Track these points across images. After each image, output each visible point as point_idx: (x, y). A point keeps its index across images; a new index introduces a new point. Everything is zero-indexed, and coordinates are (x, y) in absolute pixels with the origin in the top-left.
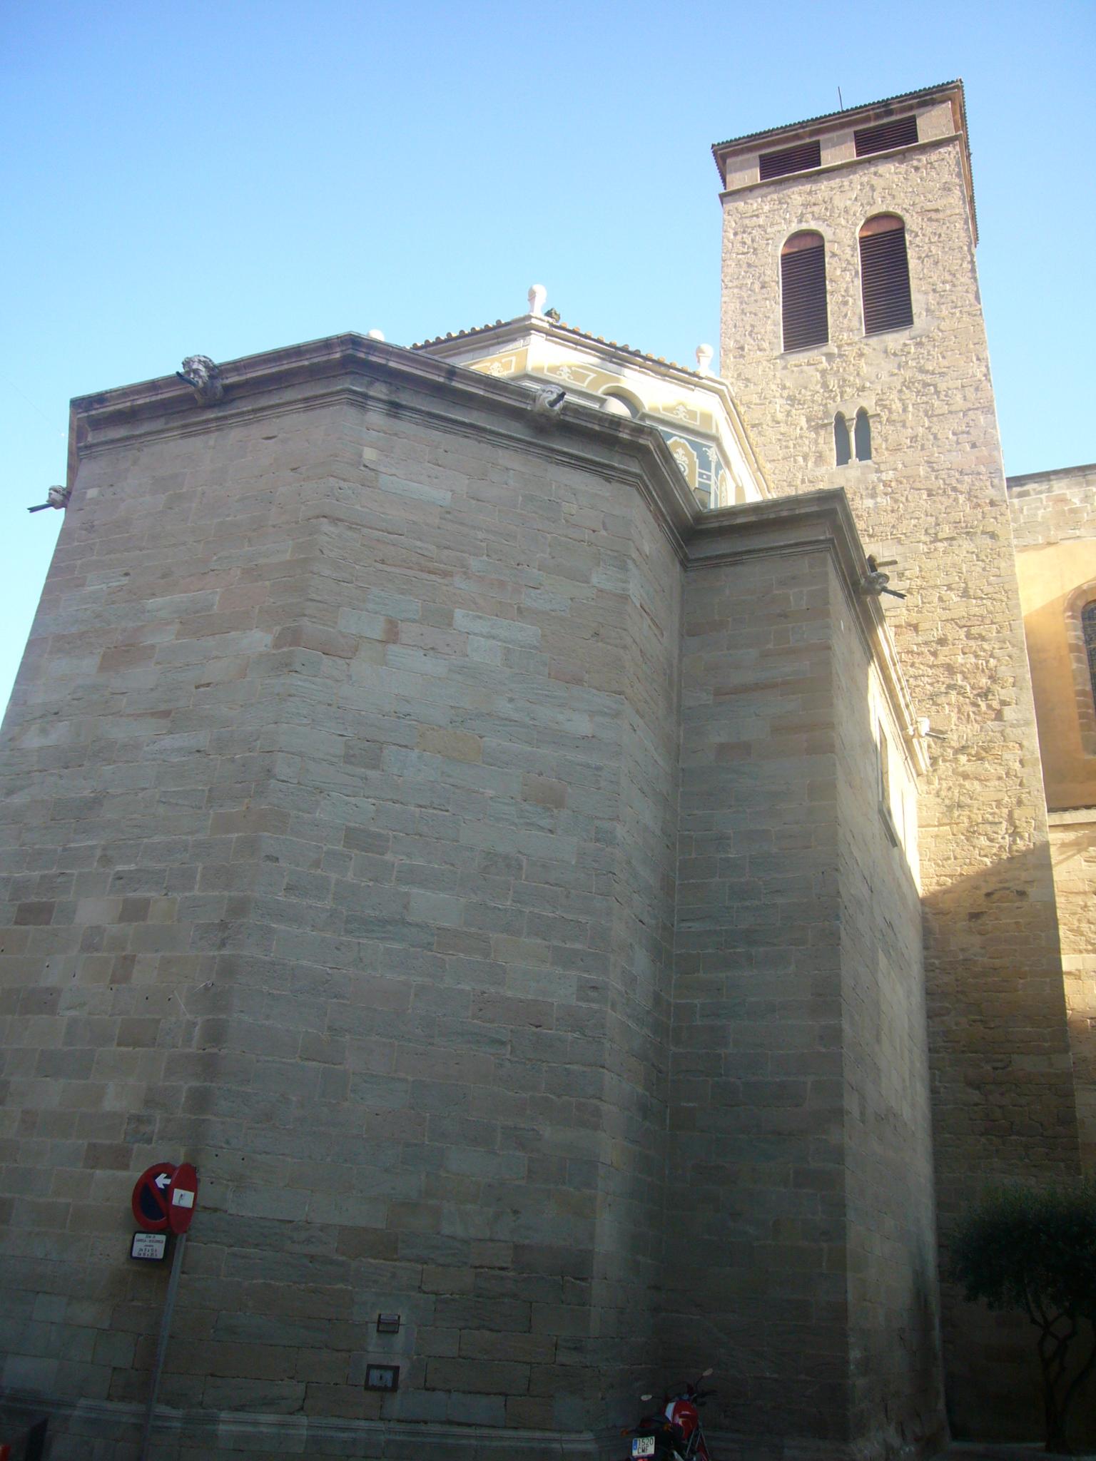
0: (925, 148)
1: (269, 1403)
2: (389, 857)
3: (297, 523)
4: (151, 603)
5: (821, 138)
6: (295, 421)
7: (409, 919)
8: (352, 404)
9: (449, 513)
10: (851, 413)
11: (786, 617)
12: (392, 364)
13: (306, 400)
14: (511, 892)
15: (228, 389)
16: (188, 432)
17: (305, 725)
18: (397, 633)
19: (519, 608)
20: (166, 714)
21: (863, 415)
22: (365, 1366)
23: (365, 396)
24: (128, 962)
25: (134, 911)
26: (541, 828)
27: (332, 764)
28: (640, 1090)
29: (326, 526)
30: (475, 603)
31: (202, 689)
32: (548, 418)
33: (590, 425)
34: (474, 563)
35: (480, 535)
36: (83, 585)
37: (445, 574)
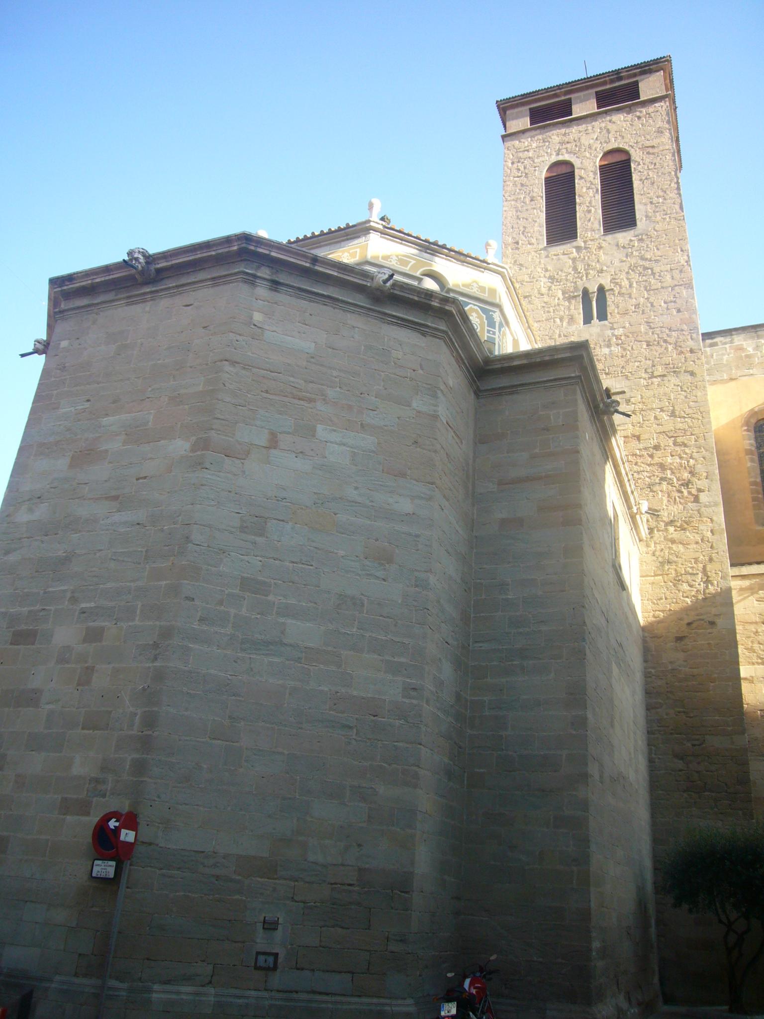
0: (645, 103)
1: (187, 979)
2: (271, 598)
3: (207, 364)
4: (105, 421)
5: (572, 96)
6: (205, 293)
7: (285, 641)
8: (245, 281)
9: (313, 358)
10: (593, 288)
11: (548, 430)
12: (273, 254)
13: (213, 279)
14: (356, 622)
15: (159, 271)
16: (131, 301)
17: (213, 506)
18: (277, 442)
19: (362, 424)
20: (116, 498)
21: (601, 290)
22: (254, 953)
23: (255, 276)
24: (90, 671)
25: (94, 636)
26: (377, 578)
27: (231, 533)
28: (446, 760)
29: (227, 367)
30: (331, 421)
31: (141, 481)
32: (382, 292)
33: (411, 297)
34: (331, 393)
35: (335, 373)
36: (58, 408)
37: (310, 400)
